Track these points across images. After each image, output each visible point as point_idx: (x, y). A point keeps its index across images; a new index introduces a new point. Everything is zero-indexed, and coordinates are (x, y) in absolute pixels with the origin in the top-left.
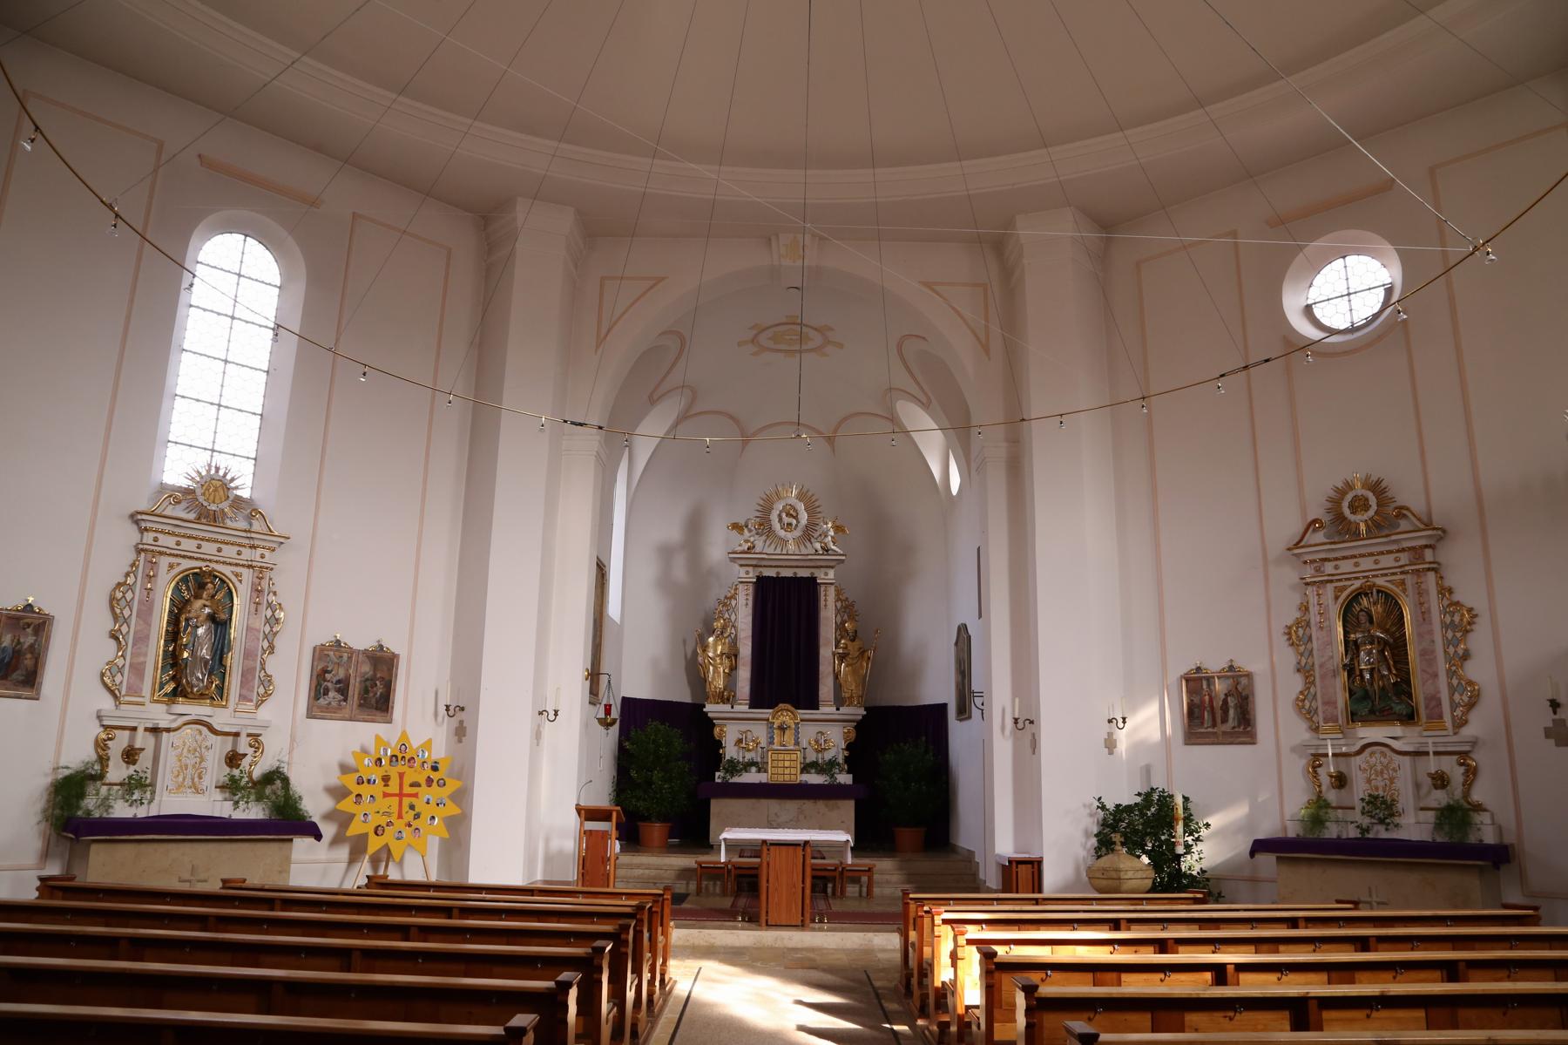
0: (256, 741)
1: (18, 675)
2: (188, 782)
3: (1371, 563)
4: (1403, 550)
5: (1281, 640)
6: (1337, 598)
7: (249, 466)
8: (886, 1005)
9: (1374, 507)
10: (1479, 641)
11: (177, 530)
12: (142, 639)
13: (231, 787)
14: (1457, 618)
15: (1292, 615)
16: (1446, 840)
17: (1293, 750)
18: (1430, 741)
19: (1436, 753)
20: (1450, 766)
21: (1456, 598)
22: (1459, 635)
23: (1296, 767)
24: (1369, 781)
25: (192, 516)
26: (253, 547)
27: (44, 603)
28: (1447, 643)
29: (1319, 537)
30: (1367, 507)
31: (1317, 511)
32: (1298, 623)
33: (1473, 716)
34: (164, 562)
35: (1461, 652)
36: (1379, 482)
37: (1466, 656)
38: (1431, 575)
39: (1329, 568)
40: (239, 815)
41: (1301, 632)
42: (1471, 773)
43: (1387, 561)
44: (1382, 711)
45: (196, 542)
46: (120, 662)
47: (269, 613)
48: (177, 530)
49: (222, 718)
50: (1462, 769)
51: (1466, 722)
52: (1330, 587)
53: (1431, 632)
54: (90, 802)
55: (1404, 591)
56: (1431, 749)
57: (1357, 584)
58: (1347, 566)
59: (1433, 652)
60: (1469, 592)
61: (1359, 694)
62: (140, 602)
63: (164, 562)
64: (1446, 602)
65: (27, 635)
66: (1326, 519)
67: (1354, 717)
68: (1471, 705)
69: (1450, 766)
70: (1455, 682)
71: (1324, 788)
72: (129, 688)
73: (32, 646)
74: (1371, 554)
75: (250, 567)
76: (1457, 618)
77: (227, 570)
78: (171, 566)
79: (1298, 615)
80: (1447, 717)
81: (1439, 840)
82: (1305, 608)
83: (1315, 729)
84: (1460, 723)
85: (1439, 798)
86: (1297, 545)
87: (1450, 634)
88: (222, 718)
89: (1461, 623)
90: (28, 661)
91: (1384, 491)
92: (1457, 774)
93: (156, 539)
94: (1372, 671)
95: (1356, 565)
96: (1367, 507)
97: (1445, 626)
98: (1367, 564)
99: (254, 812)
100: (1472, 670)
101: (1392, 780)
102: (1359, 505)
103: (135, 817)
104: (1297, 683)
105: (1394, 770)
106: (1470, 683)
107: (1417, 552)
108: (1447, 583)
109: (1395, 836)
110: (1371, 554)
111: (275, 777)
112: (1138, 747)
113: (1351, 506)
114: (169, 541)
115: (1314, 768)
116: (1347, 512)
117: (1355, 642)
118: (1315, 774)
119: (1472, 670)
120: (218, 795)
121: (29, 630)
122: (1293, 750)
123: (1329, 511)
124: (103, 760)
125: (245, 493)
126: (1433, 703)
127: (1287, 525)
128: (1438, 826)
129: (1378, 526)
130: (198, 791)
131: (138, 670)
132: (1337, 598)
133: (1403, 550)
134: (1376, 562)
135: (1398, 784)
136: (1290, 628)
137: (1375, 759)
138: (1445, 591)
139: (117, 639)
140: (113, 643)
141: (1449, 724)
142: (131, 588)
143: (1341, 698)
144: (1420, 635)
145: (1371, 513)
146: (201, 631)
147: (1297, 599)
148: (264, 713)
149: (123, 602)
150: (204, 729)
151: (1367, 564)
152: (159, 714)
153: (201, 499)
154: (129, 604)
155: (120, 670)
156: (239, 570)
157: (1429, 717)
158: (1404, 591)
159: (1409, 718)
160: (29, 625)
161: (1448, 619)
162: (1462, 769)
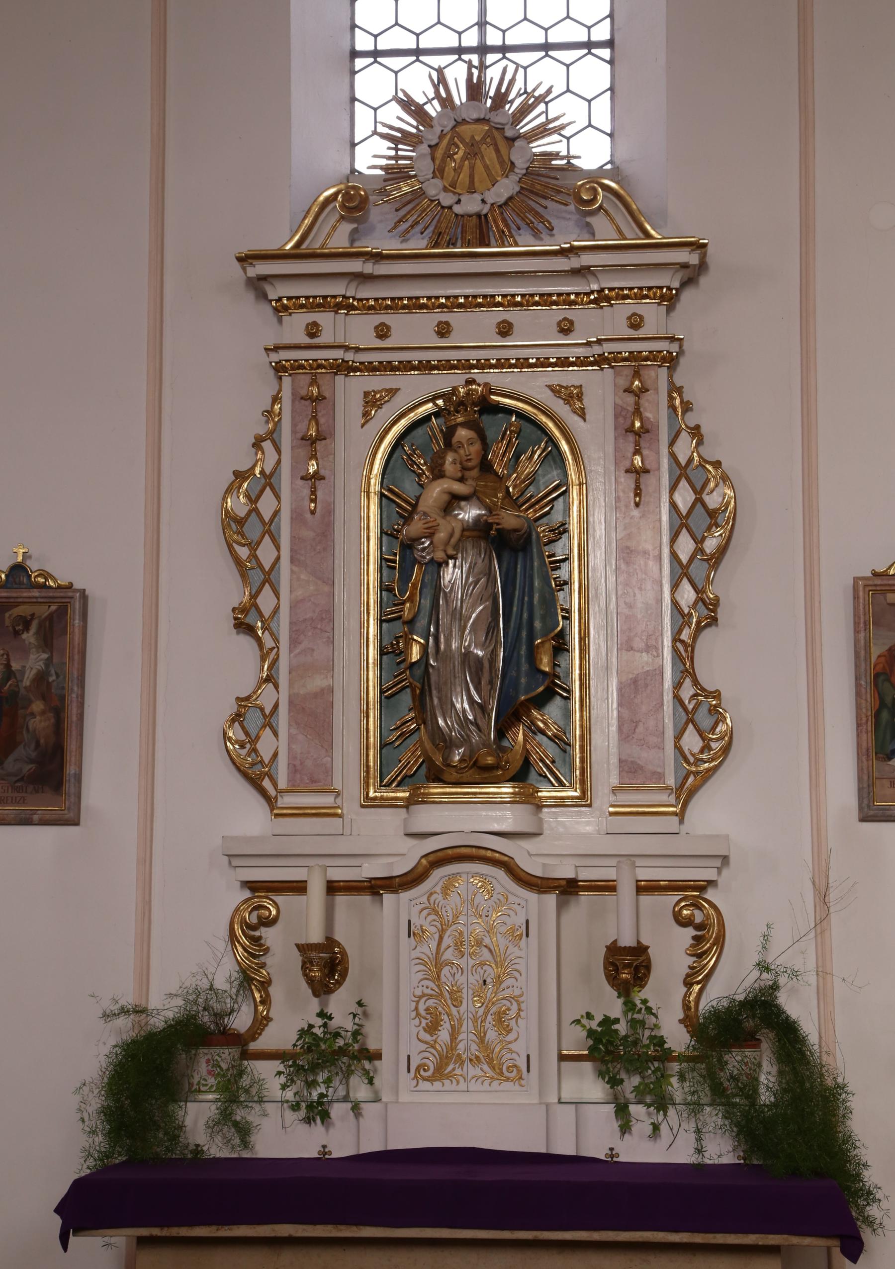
0: (693, 903)
1: (19, 762)
2: (467, 1043)
7: (594, 74)
8: (732, 494)
11: (368, 292)
12: (318, 622)
13: (615, 1052)
25: (418, 244)
26: (602, 298)
27: (62, 566)
34: (349, 392)
40: (638, 1150)
45: (430, 320)
46: (267, 697)
47: (684, 498)
48: (368, 292)
49: (572, 832)
54: (197, 1119)
62: (297, 517)
63: (349, 392)
65: (25, 651)
72: (294, 770)
73: (41, 678)
74: (431, 305)
75: (600, 361)
77: (535, 386)
78: (372, 402)
88: (572, 832)
90: (39, 722)
93: (313, 330)
99: (682, 1139)
103: (323, 1161)
110: (431, 305)
111: (758, 1018)
112: (193, 1093)
114: (359, 330)
120: (586, 1084)
121: (29, 637)
124: (251, 980)
125: (591, 152)
130: (500, 1070)
131: (315, 716)
139: (250, 630)
140: (245, 642)
142: (270, 481)
146: (452, 574)
148: (716, 814)
149: (253, 529)
150: (500, 874)
152: (383, 839)
153: (434, 188)
154: (270, 529)
155: (269, 721)
156: (571, 377)
160: (26, 623)
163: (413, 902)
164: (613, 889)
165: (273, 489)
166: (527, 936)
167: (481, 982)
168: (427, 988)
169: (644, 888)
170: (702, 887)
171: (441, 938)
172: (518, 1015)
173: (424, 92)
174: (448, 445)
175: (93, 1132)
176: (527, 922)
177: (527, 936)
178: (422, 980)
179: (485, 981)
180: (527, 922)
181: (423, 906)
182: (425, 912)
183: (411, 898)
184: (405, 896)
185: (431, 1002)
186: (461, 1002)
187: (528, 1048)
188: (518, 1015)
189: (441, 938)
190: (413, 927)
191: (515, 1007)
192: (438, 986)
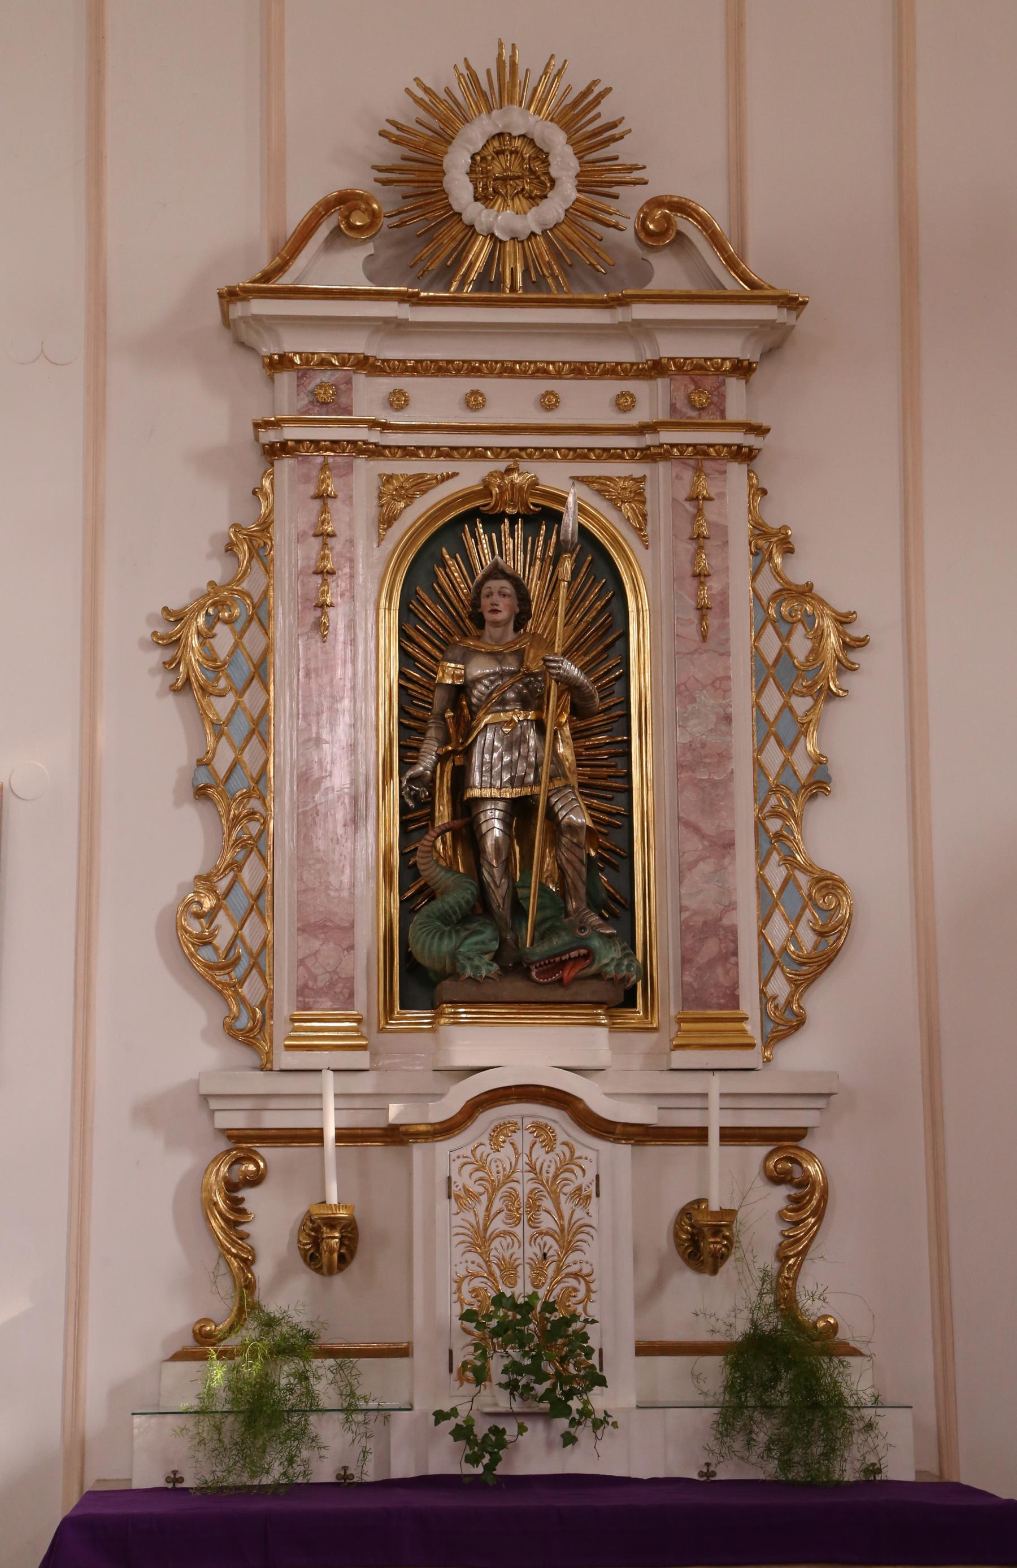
3: (505, 397)
4: (657, 369)
5: (134, 674)
6: (387, 520)
9: (567, 190)
10: (858, 732)
14: (800, 646)
15: (189, 570)
16: (759, 1468)
17: (148, 1113)
18: (715, 1085)
19: (698, 1135)
20: (726, 1178)
21: (799, 573)
22: (801, 704)
23: (153, 1186)
24: (480, 1240)
28: (766, 730)
29: (348, 267)
30: (538, 184)
31: (336, 154)
32: (217, 600)
33: (821, 1002)
35: (803, 769)
36: (590, 98)
37: (818, 785)
38: (737, 471)
39: (369, 396)
41: (224, 640)
42: (807, 1202)
43: (588, 403)
44: (554, 964)
50: (779, 1196)
51: (800, 1022)
52: (367, 472)
53: (721, 684)
55: (640, 526)
56: (715, 1121)
57: (470, 475)
58: (435, 402)
59: (723, 756)
60: (844, 564)
61: (458, 895)
64: (768, 585)
66: (385, 201)
67: (420, 983)
68: (813, 967)
69: (726, 1178)
70: (776, 874)
71: (263, 1271)
74: (539, 371)
76: (800, 646)
79: (216, 571)
80: (749, 1004)
81: (724, 1473)
82: (252, 542)
83: (250, 1034)
84: (786, 1024)
85: (720, 1305)
86: (266, 285)
87: (772, 700)
89: (811, 658)
91: (608, 134)
92: (762, 1215)
94: (520, 812)
95: (474, 401)
96: (538, 184)
97: (764, 673)
98: (511, 402)
100: (827, 837)
101: (568, 1238)
102: (514, 171)
104: (188, 842)
105: (581, 1197)
106: (829, 884)
107: (702, 380)
108: (773, 521)
109: (579, 1461)
110: (539, 371)
113: (478, 167)
115: (231, 1187)
116: (460, 190)
117: (460, 692)
118: (236, 1214)
119: (827, 837)
122: (148, 1113)
123: (388, 175)
126: (711, 948)
127: (204, 207)
128: (731, 1418)
129: (565, 268)
132: (387, 520)
133: (657, 369)
134: (549, 402)
135: (589, 1255)
136: (177, 617)
137: (512, 1150)
138: (771, 542)
141: (753, 1028)
143: (369, 905)
144: (683, 693)
145: (553, 208)
147: (217, 510)
151: (511, 402)
157: (692, 998)
158: (640, 526)
159: (620, 997)
161: (771, 645)
162: (779, 1196)
163: (454, 1155)
164: (404, 1352)
165: (262, 975)
166: (598, 1195)
167: (540, 1255)
168: (473, 1262)
169: (731, 1136)
170: (798, 1134)
171: (490, 1201)
172: (588, 1297)
173: (566, 61)
174: (220, 1440)
175: (870, 1426)
176: (597, 1177)
177: (598, 1195)
178: (464, 1253)
179: (545, 1255)
180: (597, 1177)
181: (466, 1160)
182: (469, 1168)
183: (452, 1148)
184: (443, 1147)
185: (477, 1283)
186: (516, 1282)
187: (601, 1342)
188: (588, 1297)
189: (490, 1201)
190: (453, 1187)
191: (582, 1288)
192: (486, 1262)
